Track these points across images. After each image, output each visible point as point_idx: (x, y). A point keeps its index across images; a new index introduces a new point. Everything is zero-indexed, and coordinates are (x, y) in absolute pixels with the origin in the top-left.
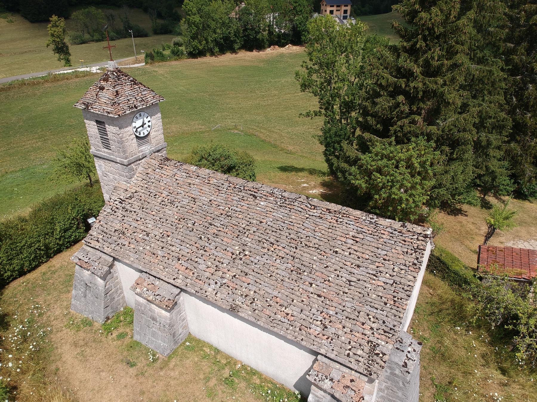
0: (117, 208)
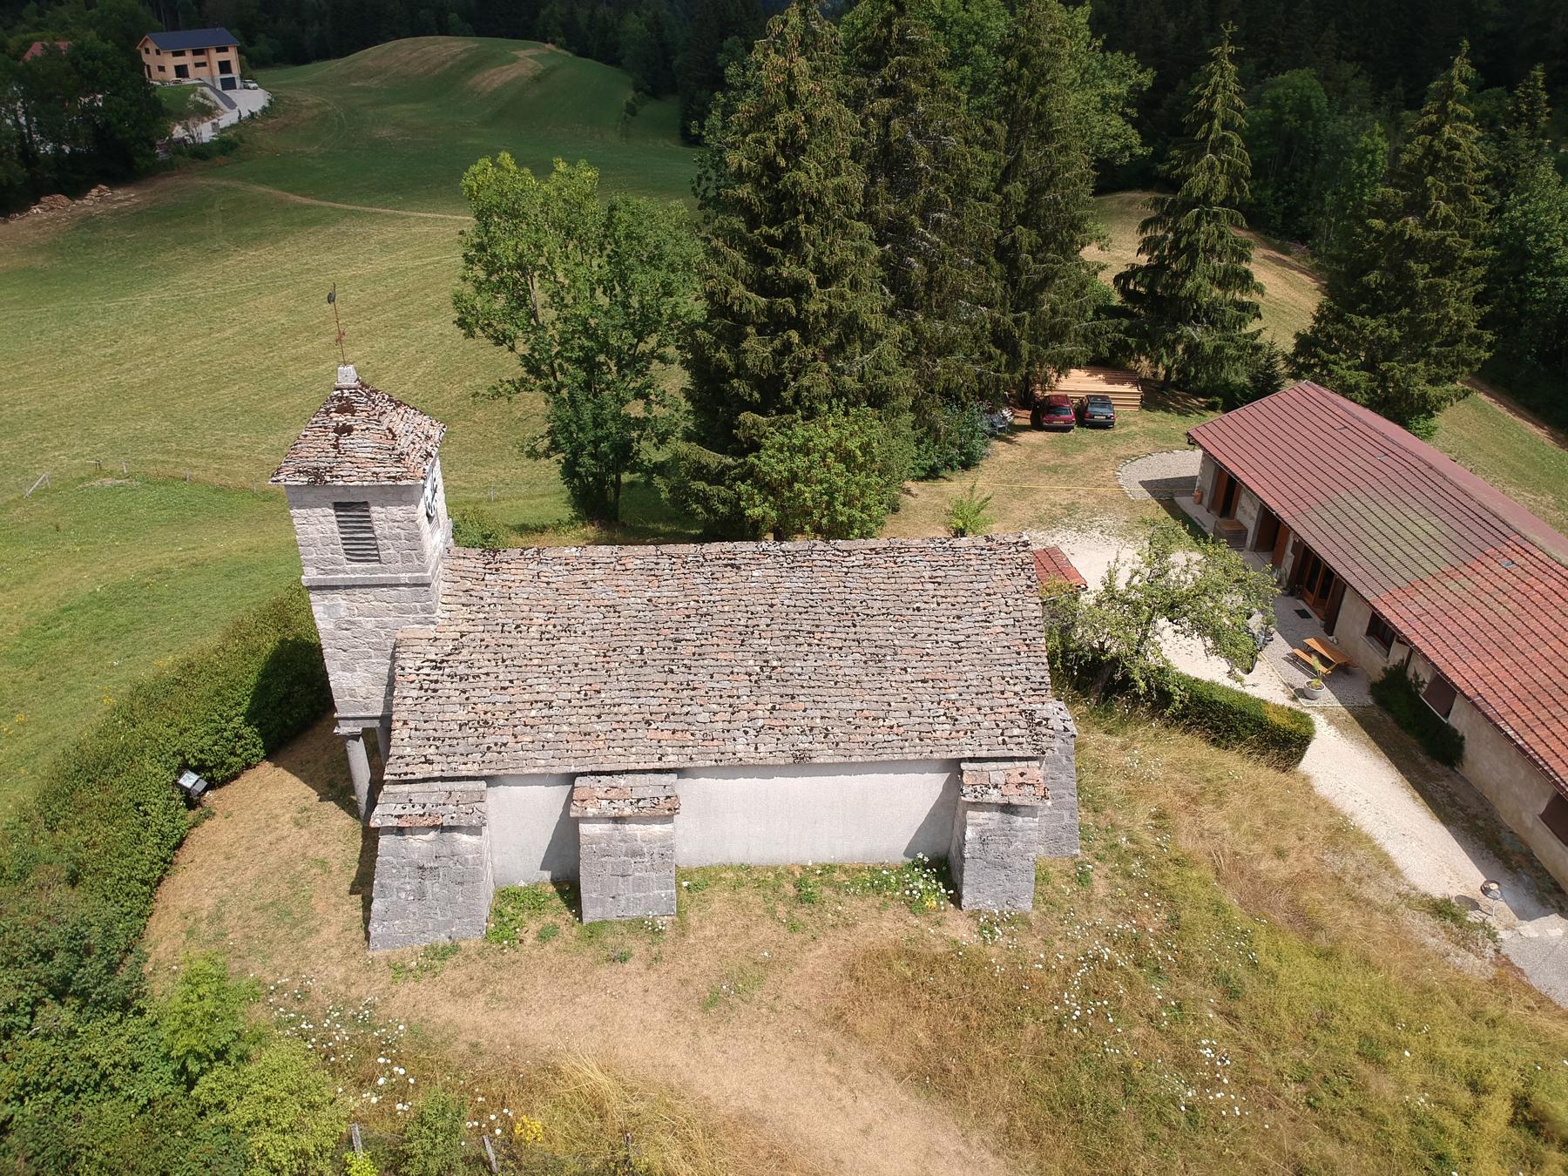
0: (436, 682)
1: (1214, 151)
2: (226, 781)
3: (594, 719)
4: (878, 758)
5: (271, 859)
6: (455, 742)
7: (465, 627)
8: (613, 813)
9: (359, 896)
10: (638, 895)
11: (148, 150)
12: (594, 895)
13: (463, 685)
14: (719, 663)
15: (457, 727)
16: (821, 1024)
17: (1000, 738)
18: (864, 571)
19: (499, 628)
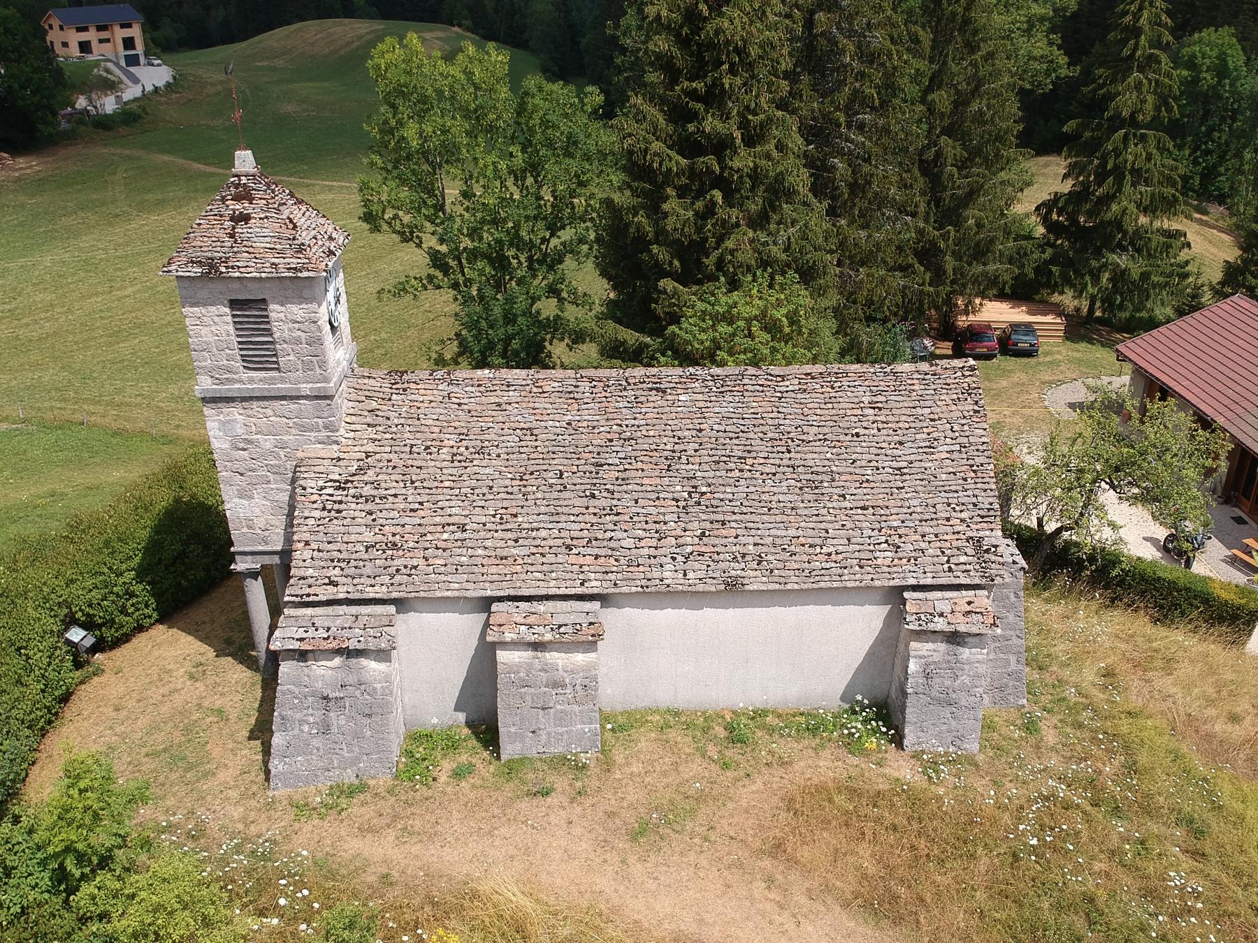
0: (340, 502)
1: (1141, 69)
2: (117, 643)
3: (510, 543)
4: (815, 586)
5: (163, 709)
6: (361, 563)
7: (370, 448)
8: (533, 638)
9: (258, 742)
10: (560, 730)
11: (50, 118)
12: (513, 730)
13: (369, 507)
14: (644, 488)
15: (362, 549)
16: (759, 853)
17: (946, 566)
18: (799, 396)
19: (407, 449)
